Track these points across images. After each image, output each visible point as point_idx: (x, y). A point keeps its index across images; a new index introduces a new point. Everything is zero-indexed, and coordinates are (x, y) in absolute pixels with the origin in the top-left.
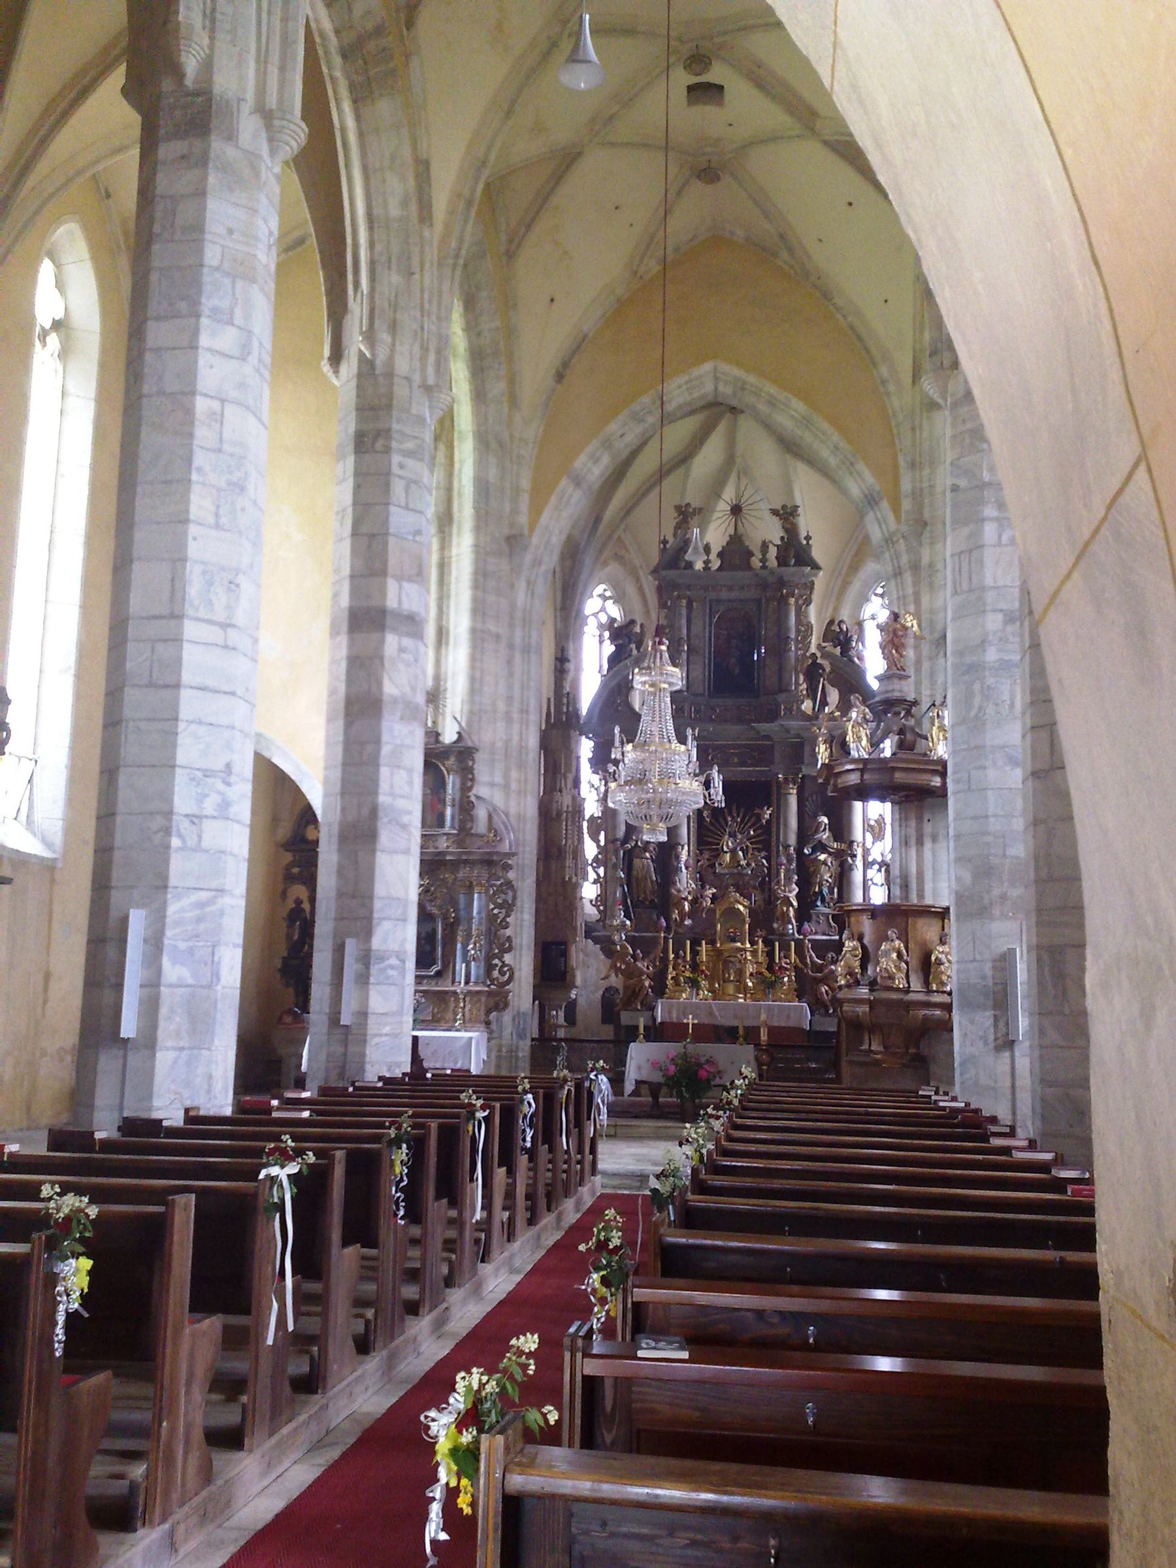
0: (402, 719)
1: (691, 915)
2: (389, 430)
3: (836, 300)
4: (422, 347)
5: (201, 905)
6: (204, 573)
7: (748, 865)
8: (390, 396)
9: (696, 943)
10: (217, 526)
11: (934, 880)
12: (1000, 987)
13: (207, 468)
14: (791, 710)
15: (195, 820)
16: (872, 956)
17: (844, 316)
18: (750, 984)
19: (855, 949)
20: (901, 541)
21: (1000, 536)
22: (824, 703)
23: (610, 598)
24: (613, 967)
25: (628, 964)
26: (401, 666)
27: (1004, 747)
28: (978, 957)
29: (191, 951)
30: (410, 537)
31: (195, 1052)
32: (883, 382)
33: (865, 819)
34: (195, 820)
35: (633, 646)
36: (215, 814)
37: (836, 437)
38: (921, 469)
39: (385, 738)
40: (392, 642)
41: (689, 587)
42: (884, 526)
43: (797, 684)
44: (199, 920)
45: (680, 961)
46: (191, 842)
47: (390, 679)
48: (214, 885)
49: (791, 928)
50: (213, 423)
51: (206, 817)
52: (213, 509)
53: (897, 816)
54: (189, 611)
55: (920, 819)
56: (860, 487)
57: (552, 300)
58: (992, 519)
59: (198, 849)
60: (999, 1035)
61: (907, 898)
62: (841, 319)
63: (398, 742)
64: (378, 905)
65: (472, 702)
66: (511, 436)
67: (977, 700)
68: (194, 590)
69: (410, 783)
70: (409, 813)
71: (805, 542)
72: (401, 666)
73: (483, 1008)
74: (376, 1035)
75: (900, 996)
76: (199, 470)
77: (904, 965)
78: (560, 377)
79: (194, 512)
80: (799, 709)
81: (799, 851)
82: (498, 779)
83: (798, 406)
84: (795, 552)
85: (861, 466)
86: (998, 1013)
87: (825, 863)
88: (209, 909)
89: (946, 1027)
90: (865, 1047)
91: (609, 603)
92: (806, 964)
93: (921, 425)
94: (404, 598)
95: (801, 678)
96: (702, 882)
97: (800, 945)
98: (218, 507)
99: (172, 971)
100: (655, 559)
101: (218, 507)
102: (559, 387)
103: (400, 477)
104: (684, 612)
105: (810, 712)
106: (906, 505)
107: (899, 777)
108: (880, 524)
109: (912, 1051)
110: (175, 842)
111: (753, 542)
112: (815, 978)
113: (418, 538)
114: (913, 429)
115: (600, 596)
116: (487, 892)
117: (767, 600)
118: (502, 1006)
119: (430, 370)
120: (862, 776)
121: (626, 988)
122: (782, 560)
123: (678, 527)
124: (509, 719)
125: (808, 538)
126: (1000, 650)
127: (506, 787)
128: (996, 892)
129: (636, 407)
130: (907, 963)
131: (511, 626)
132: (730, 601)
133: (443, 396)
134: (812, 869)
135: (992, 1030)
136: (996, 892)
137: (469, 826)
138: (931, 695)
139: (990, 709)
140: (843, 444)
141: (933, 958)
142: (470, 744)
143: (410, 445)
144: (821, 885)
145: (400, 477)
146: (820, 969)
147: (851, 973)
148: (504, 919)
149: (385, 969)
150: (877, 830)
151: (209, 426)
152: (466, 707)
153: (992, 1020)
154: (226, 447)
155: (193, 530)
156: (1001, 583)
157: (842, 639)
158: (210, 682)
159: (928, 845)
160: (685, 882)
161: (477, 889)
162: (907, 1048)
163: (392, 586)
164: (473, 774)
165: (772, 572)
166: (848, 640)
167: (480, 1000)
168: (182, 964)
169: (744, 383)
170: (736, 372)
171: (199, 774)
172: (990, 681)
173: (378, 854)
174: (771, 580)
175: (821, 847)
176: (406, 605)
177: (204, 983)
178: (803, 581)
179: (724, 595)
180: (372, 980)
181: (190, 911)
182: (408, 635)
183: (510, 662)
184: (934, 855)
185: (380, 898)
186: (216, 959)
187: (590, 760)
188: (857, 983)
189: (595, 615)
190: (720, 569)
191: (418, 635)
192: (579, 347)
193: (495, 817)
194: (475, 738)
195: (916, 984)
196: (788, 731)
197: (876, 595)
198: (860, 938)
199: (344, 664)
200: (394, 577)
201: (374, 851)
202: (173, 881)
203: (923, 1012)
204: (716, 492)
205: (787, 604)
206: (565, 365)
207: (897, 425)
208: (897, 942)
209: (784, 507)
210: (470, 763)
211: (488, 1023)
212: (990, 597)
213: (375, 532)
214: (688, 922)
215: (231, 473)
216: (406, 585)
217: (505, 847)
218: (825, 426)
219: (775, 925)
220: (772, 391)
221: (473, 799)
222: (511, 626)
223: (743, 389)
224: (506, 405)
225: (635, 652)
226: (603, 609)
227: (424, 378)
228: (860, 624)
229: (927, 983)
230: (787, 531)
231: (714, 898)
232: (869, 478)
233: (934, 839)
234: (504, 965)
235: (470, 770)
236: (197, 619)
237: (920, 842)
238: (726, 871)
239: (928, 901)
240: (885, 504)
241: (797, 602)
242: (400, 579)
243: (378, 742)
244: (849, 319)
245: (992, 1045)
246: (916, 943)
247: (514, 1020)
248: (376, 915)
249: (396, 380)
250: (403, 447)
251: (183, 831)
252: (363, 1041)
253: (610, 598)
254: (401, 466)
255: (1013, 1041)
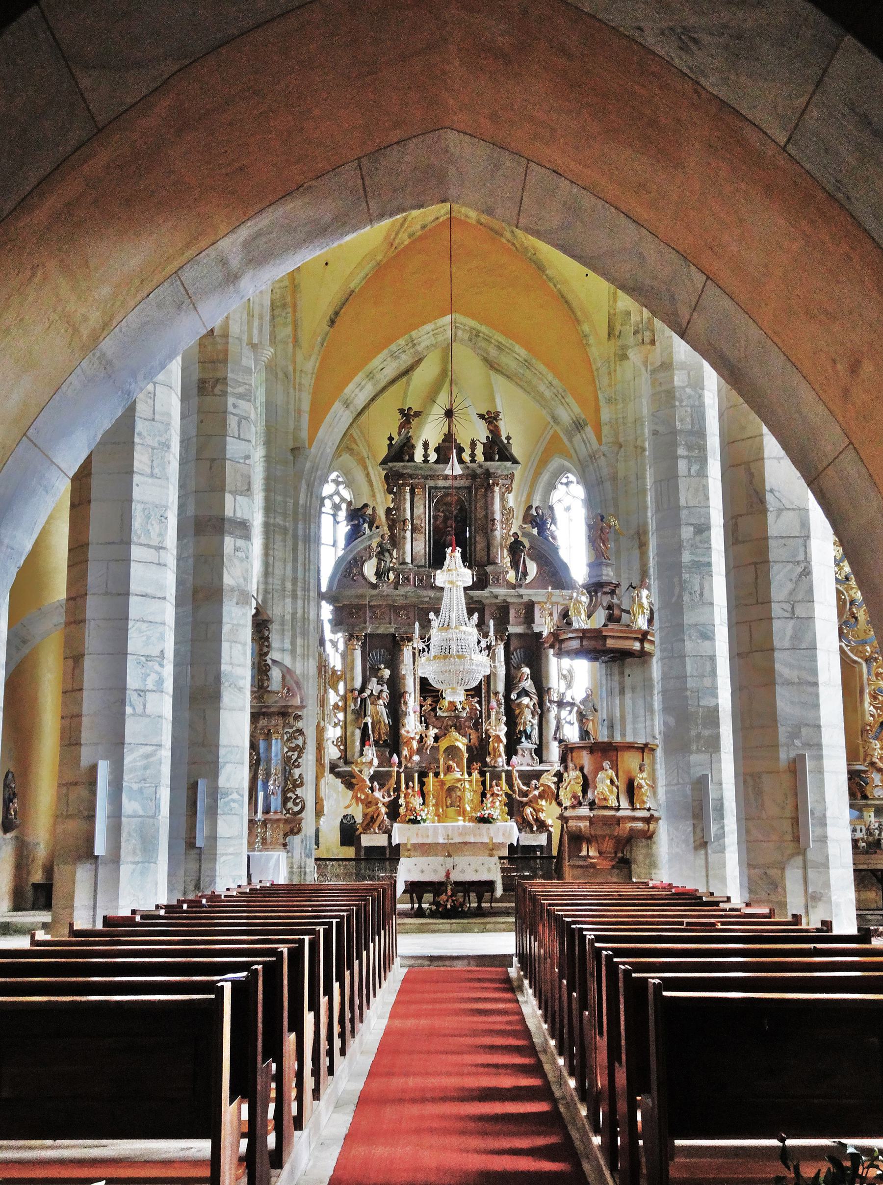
0: (237, 604)
1: (419, 751)
2: (226, 378)
3: (547, 272)
4: (248, 314)
5: (147, 756)
6: (144, 510)
7: (464, 708)
8: (226, 352)
9: (423, 775)
10: (152, 475)
11: (634, 722)
12: (697, 803)
13: (145, 434)
14: (498, 580)
15: (142, 694)
16: (590, 782)
17: (555, 286)
18: (468, 809)
19: (577, 777)
20: (602, 457)
21: (689, 470)
22: (525, 574)
23: (343, 483)
24: (355, 797)
25: (367, 796)
26: (236, 561)
27: (696, 625)
28: (681, 781)
29: (141, 790)
30: (242, 461)
31: (146, 864)
32: (586, 336)
33: (559, 669)
34: (142, 694)
35: (366, 525)
36: (155, 688)
37: (550, 377)
38: (616, 404)
39: (225, 619)
40: (229, 542)
41: (411, 476)
42: (588, 445)
43: (503, 558)
44: (145, 768)
45: (410, 791)
46: (139, 710)
47: (229, 573)
48: (154, 742)
49: (501, 761)
50: (149, 400)
51: (148, 690)
52: (150, 463)
53: (604, 672)
54: (134, 538)
55: (622, 673)
56: (569, 415)
57: (327, 264)
58: (683, 457)
59: (144, 715)
60: (697, 838)
61: (612, 736)
62: (552, 286)
63: (235, 622)
64: (222, 752)
65: (266, 583)
66: (294, 369)
67: (677, 591)
68: (137, 523)
69: (245, 654)
70: (244, 678)
71: (505, 441)
72: (236, 561)
73: (282, 833)
74: (223, 854)
75: (612, 813)
76: (139, 434)
77: (615, 789)
78: (332, 322)
79: (137, 466)
80: (504, 578)
81: (507, 697)
82: (287, 645)
83: (522, 352)
84: (497, 448)
85: (570, 399)
86: (695, 822)
87: (527, 706)
88: (151, 760)
89: (649, 836)
90: (584, 853)
91: (341, 487)
92: (514, 791)
93: (615, 371)
94: (238, 509)
95: (506, 552)
96: (425, 720)
97: (509, 775)
98: (152, 461)
99: (129, 806)
100: (383, 452)
101: (152, 461)
102: (332, 330)
103: (234, 415)
104: (408, 496)
105: (513, 581)
106: (605, 430)
107: (610, 643)
108: (585, 444)
109: (620, 855)
110: (129, 710)
111: (463, 438)
112: (522, 802)
113: (247, 461)
114: (610, 373)
115: (333, 481)
116: (282, 738)
117: (477, 489)
118: (296, 831)
119: (255, 332)
120: (581, 642)
121: (365, 815)
122: (488, 457)
123: (402, 426)
124: (294, 597)
125: (508, 438)
126: (692, 554)
127: (293, 652)
128: (693, 733)
129: (393, 347)
130: (617, 787)
131: (295, 521)
132: (444, 488)
133: (265, 352)
134: (517, 712)
135: (692, 835)
136: (693, 733)
137: (265, 685)
138: (628, 578)
139: (686, 598)
140: (556, 382)
141: (636, 784)
142: (265, 618)
143: (241, 390)
144: (525, 724)
145: (234, 415)
146: (525, 794)
147: (575, 797)
148: (296, 760)
149: (228, 802)
150: (568, 679)
151: (146, 403)
152: (262, 587)
153: (691, 828)
154: (157, 417)
155: (136, 479)
156: (691, 504)
157: (538, 520)
158: (149, 591)
159: (628, 695)
160: (412, 726)
161: (274, 736)
162: (616, 853)
163: (229, 498)
164: (268, 642)
165: (481, 466)
166: (544, 523)
167: (278, 827)
168: (136, 800)
169: (479, 332)
170: (472, 323)
171: (143, 659)
172: (686, 576)
173: (221, 711)
174: (479, 471)
175: (525, 693)
176: (239, 515)
177: (150, 814)
178: (505, 473)
179: (441, 483)
180: (219, 811)
181: (139, 761)
182: (241, 537)
183: (295, 550)
184: (633, 704)
185: (224, 746)
186: (158, 796)
187: (329, 621)
188: (580, 804)
189: (330, 497)
190: (437, 462)
191: (247, 537)
192: (347, 299)
193: (288, 677)
194: (269, 612)
195: (624, 803)
196: (496, 597)
197: (561, 483)
198: (582, 769)
199: (191, 561)
200: (230, 492)
201: (218, 709)
202: (128, 740)
203: (630, 825)
204: (432, 398)
205: (493, 492)
206: (337, 314)
207: (597, 370)
208: (610, 771)
209: (488, 412)
210: (266, 633)
211: (285, 845)
212: (684, 513)
213: (215, 457)
214: (416, 758)
215: (161, 436)
216: (238, 497)
217: (297, 701)
218: (542, 367)
219: (488, 760)
220: (500, 340)
221: (269, 662)
222: (295, 521)
223: (477, 336)
224: (291, 345)
225: (367, 531)
226: (337, 493)
227: (250, 337)
228: (551, 508)
229: (632, 802)
230: (491, 431)
231: (437, 738)
232: (577, 409)
233: (633, 689)
234: (297, 797)
235: (267, 639)
236: (141, 545)
237: (622, 692)
238: (445, 714)
239: (629, 739)
240: (589, 429)
241: (501, 489)
242: (234, 493)
243: (220, 622)
244: (558, 286)
245: (692, 846)
246: (624, 772)
247: (302, 842)
248: (221, 760)
249: (230, 340)
250: (236, 391)
251: (133, 702)
252: (214, 859)
253: (343, 483)
254: (235, 406)
255: (707, 843)
